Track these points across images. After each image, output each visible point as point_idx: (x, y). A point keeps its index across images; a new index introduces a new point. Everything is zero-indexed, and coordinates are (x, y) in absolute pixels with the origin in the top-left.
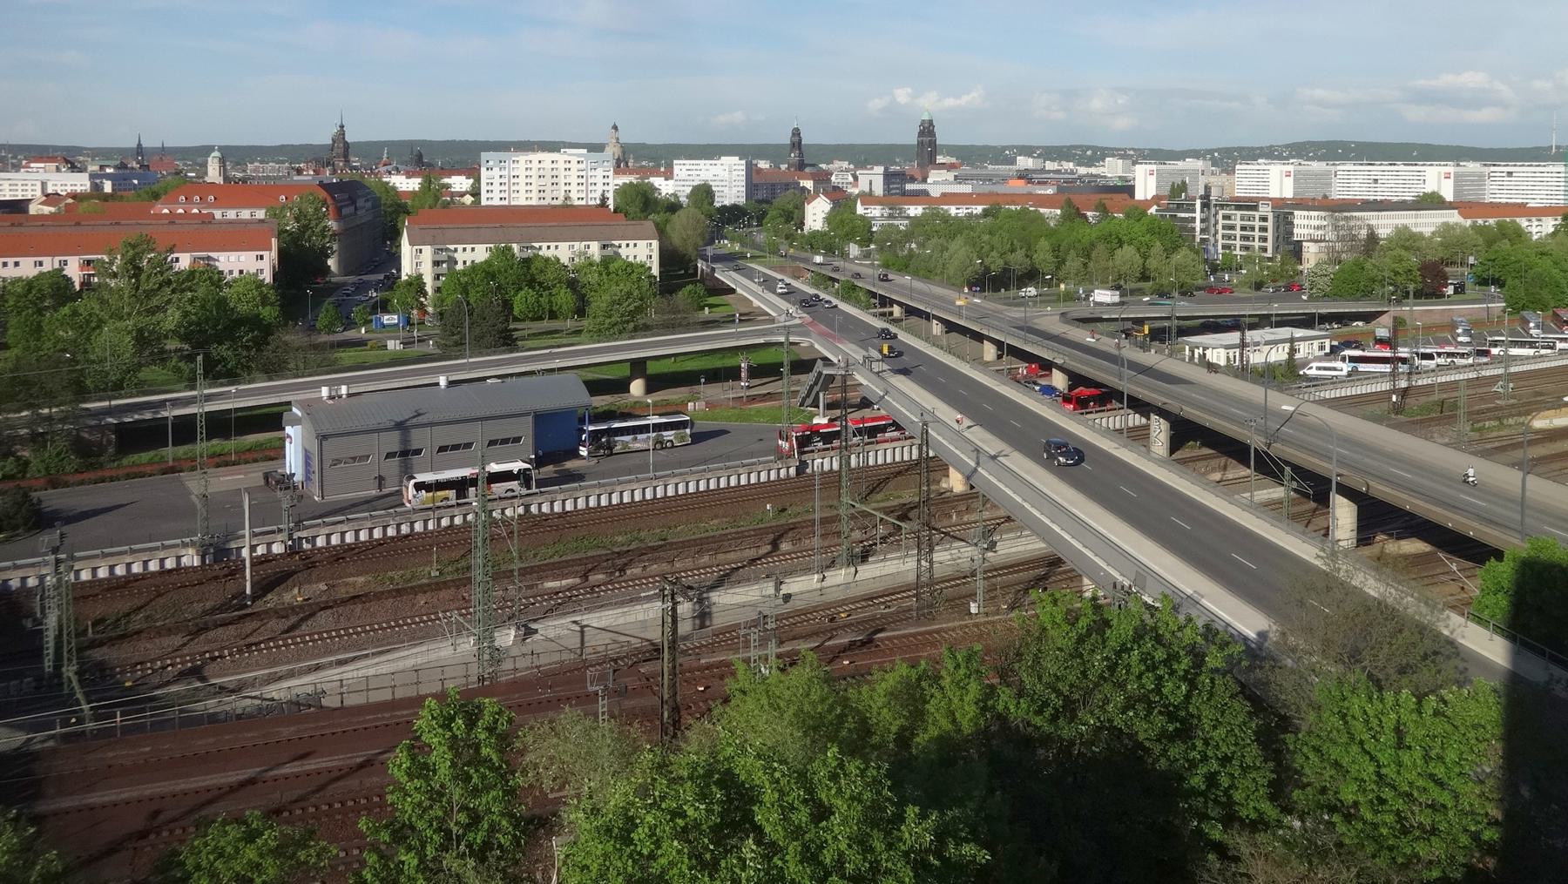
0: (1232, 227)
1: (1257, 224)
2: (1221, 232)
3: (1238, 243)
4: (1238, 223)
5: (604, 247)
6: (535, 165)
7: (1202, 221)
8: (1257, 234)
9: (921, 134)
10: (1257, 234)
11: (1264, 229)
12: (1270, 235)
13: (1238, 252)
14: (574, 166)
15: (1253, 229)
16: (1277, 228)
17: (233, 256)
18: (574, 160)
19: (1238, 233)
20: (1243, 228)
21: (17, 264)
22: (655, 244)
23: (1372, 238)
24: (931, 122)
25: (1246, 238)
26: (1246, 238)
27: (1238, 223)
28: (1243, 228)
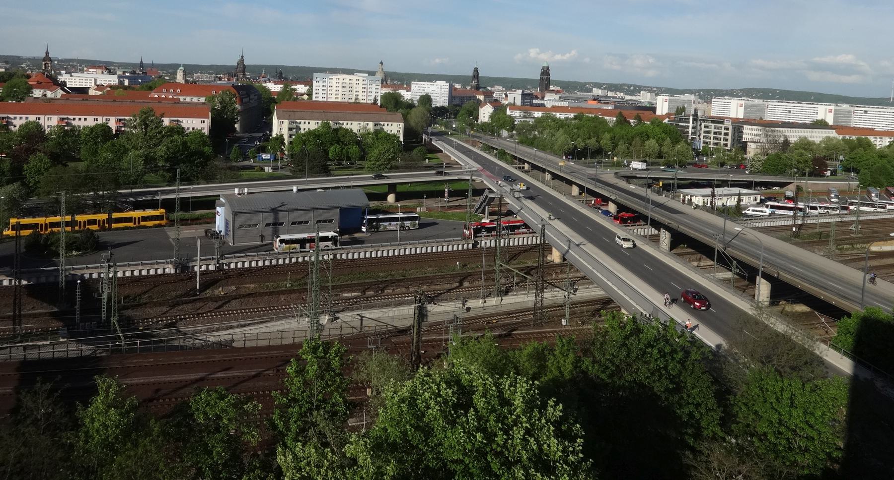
0: (709, 132)
1: (723, 131)
2: (703, 134)
3: (712, 141)
4: (713, 130)
5: (376, 125)
6: (341, 81)
7: (693, 128)
8: (722, 136)
9: (542, 74)
10: (722, 136)
11: (726, 134)
12: (729, 137)
13: (711, 146)
14: (361, 82)
15: (125, 337)
16: (734, 134)
17: (190, 120)
18: (361, 79)
19: (712, 135)
20: (715, 133)
21: (85, 119)
22: (402, 125)
23: (786, 142)
24: (548, 68)
25: (716, 139)
26: (716, 139)
27: (713, 130)
28: (715, 133)
